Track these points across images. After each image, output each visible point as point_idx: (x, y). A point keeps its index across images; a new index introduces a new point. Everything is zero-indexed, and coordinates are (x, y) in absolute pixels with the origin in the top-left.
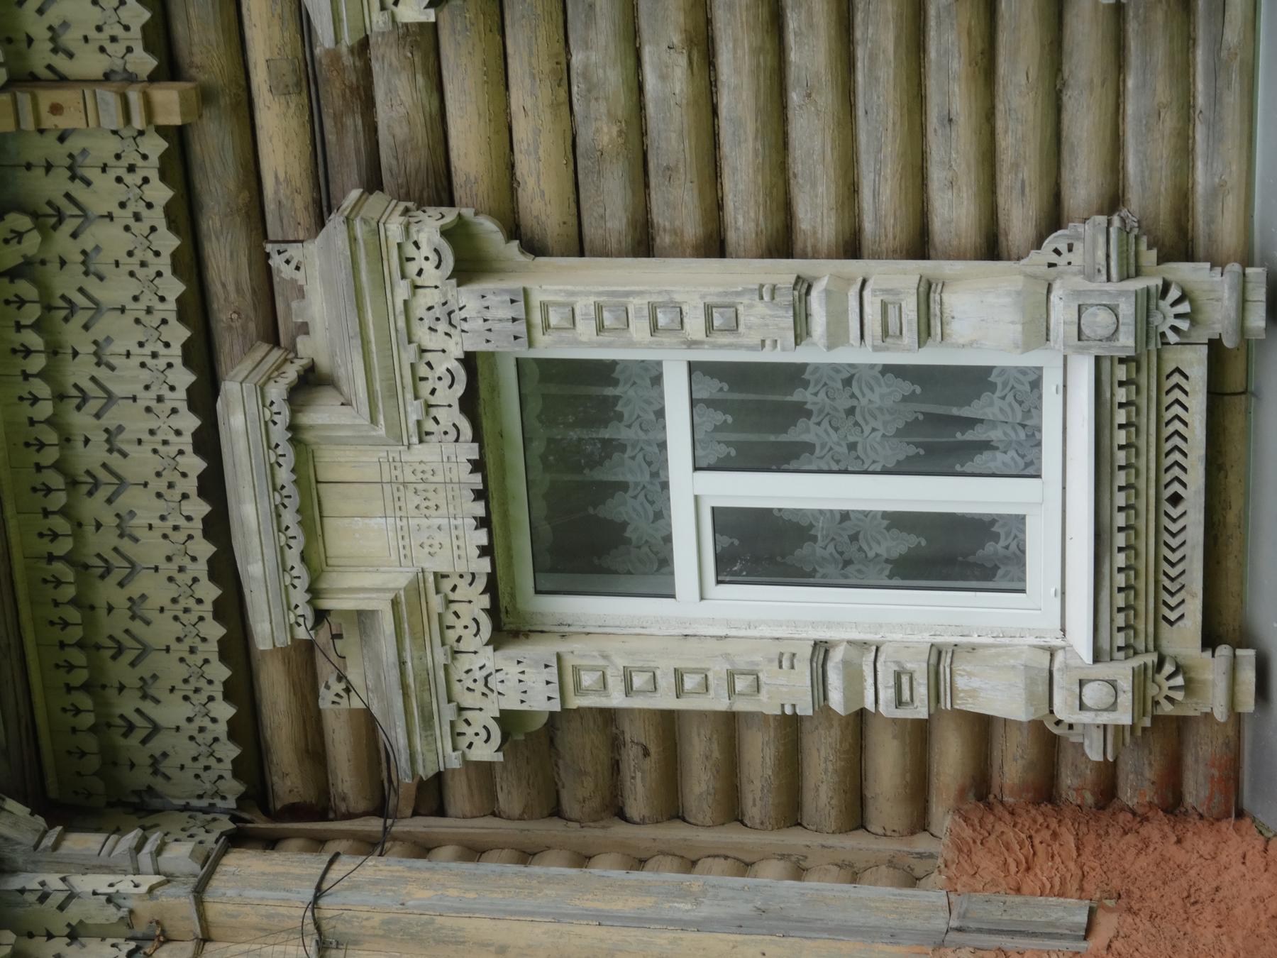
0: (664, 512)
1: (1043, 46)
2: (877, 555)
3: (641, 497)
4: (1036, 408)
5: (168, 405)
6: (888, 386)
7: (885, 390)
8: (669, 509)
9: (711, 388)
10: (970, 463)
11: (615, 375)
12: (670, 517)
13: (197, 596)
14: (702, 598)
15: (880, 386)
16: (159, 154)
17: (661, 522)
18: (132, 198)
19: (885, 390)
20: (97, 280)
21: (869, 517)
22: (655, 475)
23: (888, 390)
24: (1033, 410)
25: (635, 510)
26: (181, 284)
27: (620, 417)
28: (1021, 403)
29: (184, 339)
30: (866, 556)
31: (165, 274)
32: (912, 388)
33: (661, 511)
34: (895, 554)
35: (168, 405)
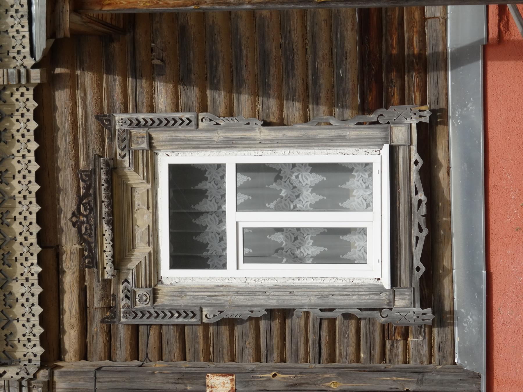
0: (223, 220)
1: (381, 340)
2: (308, 254)
3: (213, 201)
4: (371, 185)
5: (33, 343)
6: (313, 177)
7: (312, 179)
8: (226, 236)
9: (244, 178)
10: (345, 202)
11: (206, 175)
12: (226, 240)
13: (29, 169)
14: (238, 269)
15: (310, 178)
16: (36, 170)
17: (222, 242)
18: (16, 23)
19: (312, 179)
20: (4, 144)
21: (304, 165)
22: (220, 207)
23: (314, 179)
24: (370, 203)
25: (211, 220)
26: (42, 329)
27: (206, 179)
28: (365, 183)
29: (38, 252)
30: (303, 255)
31: (30, 99)
32: (323, 178)
33: (222, 237)
34: (315, 254)
35: (33, 343)
